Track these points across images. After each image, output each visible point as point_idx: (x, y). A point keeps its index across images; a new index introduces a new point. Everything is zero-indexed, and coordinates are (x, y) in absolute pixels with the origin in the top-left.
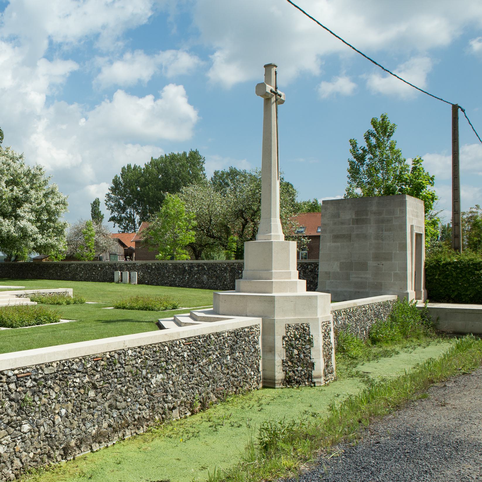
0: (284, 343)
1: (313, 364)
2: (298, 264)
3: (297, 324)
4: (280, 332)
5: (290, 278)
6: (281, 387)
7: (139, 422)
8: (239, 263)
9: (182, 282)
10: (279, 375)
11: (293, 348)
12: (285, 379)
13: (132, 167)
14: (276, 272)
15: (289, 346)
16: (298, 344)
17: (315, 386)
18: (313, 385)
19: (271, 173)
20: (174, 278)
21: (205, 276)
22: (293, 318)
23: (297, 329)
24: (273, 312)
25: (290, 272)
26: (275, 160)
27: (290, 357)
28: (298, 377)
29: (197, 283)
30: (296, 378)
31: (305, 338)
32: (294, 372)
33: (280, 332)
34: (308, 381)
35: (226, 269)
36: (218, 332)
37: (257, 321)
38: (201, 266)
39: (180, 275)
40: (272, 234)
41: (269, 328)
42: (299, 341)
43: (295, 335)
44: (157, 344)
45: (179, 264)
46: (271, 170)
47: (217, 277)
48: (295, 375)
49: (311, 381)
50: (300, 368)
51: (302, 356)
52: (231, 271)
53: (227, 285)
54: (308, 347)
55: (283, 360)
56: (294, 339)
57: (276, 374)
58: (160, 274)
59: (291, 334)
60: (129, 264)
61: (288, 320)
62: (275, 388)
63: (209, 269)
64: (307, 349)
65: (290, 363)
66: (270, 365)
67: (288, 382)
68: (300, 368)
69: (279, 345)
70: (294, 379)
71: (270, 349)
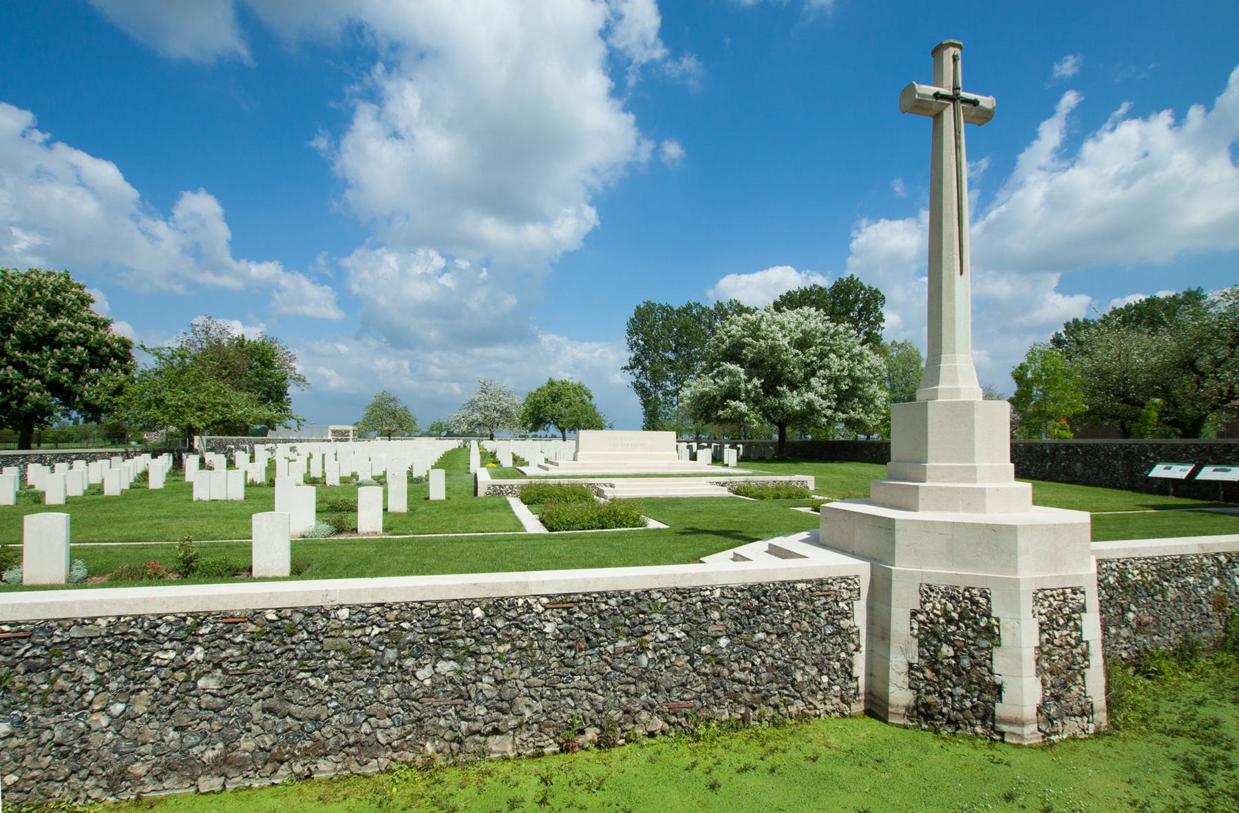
0: (916, 626)
1: (999, 689)
2: (1014, 448)
3: (955, 588)
4: (903, 601)
5: (974, 480)
6: (901, 722)
8: (1141, 445)
10: (900, 695)
11: (940, 640)
12: (916, 707)
14: (936, 467)
15: (929, 636)
16: (953, 633)
17: (1002, 741)
18: (997, 737)
19: (941, 262)
21: (1079, 465)
22: (943, 572)
23: (952, 598)
24: (891, 556)
25: (975, 467)
26: (951, 235)
28: (954, 709)
29: (1066, 474)
30: (945, 710)
31: (977, 623)
32: (941, 696)
33: (903, 601)
34: (983, 725)
35: (1116, 453)
36: (679, 586)
37: (861, 569)
38: (1073, 448)
40: (940, 387)
41: (881, 589)
42: (959, 628)
43: (946, 613)
44: (440, 601)
45: (1036, 444)
46: (941, 257)
47: (1099, 467)
48: (945, 704)
49: (993, 728)
50: (960, 691)
51: (966, 662)
52: (1125, 458)
53: (1117, 479)
54: (984, 644)
55: (911, 666)
56: (942, 620)
57: (891, 689)
59: (934, 607)
61: (929, 575)
62: (885, 721)
63: (1085, 453)
65: (929, 674)
66: (878, 669)
67: (922, 713)
68: (960, 691)
69: (901, 626)
70: (941, 713)
71: (880, 631)
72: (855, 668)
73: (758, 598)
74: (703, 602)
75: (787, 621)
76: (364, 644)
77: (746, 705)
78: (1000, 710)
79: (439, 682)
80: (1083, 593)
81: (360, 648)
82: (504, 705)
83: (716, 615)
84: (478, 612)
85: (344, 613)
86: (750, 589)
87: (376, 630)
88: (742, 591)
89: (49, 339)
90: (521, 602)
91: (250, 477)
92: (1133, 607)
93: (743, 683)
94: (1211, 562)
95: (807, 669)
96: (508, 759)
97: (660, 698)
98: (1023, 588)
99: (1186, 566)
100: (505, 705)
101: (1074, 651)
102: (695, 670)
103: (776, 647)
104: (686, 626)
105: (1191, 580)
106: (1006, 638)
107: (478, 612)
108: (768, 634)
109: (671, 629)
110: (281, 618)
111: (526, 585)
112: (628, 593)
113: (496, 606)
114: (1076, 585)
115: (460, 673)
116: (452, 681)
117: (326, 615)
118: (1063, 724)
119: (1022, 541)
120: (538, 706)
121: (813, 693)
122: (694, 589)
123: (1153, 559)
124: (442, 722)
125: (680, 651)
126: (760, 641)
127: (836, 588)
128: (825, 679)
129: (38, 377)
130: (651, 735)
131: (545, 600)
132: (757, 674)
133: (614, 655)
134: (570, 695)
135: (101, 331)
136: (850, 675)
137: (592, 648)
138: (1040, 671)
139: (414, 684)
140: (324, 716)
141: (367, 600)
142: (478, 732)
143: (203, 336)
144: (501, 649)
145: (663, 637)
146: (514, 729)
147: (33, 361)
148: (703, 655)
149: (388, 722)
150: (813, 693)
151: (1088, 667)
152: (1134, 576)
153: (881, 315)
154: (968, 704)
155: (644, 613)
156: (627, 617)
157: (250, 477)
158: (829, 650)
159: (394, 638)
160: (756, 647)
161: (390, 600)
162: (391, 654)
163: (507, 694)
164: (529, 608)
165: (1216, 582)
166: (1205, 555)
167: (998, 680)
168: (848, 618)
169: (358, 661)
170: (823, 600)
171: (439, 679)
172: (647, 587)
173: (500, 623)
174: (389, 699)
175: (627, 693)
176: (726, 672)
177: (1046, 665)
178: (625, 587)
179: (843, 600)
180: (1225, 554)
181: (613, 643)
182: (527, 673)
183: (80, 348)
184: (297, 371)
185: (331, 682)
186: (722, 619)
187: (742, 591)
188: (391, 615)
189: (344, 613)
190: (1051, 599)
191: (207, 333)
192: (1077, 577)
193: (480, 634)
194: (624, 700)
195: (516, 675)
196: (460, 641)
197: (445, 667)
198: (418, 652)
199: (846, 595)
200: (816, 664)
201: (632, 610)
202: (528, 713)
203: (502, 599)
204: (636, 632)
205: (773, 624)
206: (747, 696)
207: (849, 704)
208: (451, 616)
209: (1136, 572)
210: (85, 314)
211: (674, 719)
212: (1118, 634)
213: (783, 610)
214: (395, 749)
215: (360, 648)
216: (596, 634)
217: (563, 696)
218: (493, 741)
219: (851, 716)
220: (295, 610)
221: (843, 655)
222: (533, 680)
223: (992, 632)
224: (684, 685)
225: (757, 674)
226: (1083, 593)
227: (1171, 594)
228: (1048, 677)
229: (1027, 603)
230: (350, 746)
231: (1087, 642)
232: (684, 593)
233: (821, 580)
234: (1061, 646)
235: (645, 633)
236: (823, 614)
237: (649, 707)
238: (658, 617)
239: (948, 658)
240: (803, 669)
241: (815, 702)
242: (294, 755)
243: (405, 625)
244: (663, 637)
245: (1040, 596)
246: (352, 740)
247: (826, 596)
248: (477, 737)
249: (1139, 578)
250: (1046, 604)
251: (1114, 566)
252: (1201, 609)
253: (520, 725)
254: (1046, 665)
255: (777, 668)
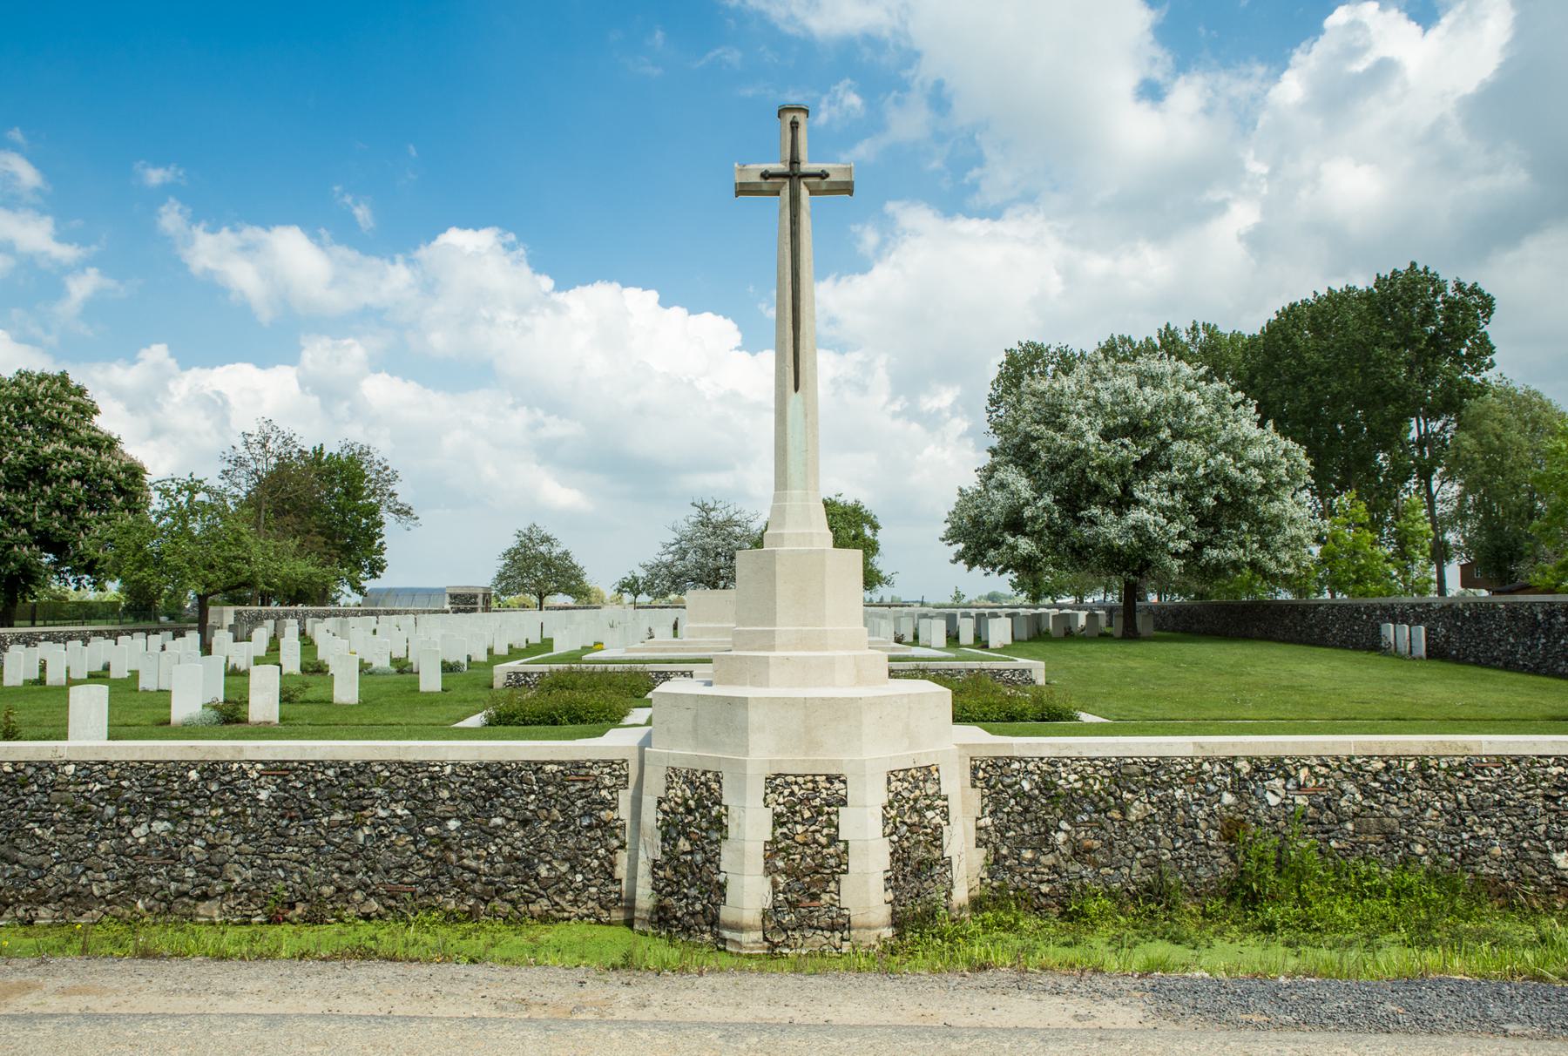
1: (722, 887)
7: (78, 899)
9: (1532, 658)
13: (1420, 268)
15: (670, 830)
20: (1513, 646)
27: (671, 857)
39: (1525, 635)
50: (693, 892)
54: (715, 836)
58: (1480, 631)
60: (1419, 605)
61: (674, 757)
64: (711, 843)
67: (662, 918)
72: (618, 869)
73: (496, 778)
74: (431, 778)
75: (532, 807)
76: (86, 799)
77: (475, 897)
78: (726, 914)
79: (153, 840)
80: (844, 782)
81: (82, 802)
82: (212, 868)
83: (445, 794)
84: (193, 775)
85: (71, 769)
86: (487, 767)
87: (98, 786)
88: (478, 769)
89: (38, 471)
90: (236, 766)
91: (231, 662)
92: (1064, 825)
93: (475, 871)
94: (1217, 769)
95: (555, 863)
96: (214, 924)
97: (376, 878)
98: (749, 771)
99: (1168, 772)
100: (215, 869)
101: (825, 851)
102: (418, 852)
103: (517, 835)
104: (410, 804)
105: (1179, 793)
106: (732, 832)
107: (193, 775)
108: (509, 820)
109: (393, 806)
110: (16, 771)
111: (241, 750)
112: (347, 763)
113: (211, 770)
114: (834, 772)
115: (173, 833)
116: (165, 842)
117: (54, 769)
118: (804, 937)
119: (754, 716)
120: (249, 874)
121: (562, 892)
122: (421, 763)
123: (1104, 760)
124: (153, 881)
125: (402, 830)
126: (496, 827)
127: (596, 773)
128: (579, 877)
129: (23, 526)
130: (367, 917)
131: (259, 766)
132: (492, 863)
133: (329, 827)
134: (281, 866)
135: (104, 458)
136: (611, 875)
137: (305, 819)
138: (770, 870)
139: (129, 841)
140: (46, 865)
141: (92, 758)
142: (186, 894)
143: (258, 450)
144: (214, 813)
145: (382, 813)
146: (222, 895)
147: (19, 504)
148: (429, 837)
149: (104, 876)
150: (562, 892)
151: (846, 872)
152: (1068, 780)
153: (1484, 339)
154: (698, 907)
155: (364, 786)
156: (344, 789)
157: (231, 662)
158: (585, 844)
159: (114, 794)
160: (492, 834)
161: (112, 758)
162: (110, 810)
163: (217, 858)
164: (244, 774)
165: (1228, 798)
166: (1206, 759)
167: (721, 878)
168: (612, 810)
169: (80, 814)
170: (579, 785)
171: (152, 838)
172: (368, 758)
173: (214, 787)
174: (107, 854)
175: (339, 869)
176: (453, 857)
177: (781, 864)
178: (344, 758)
179: (605, 787)
180: (1250, 760)
181: (329, 815)
182: (238, 840)
183: (75, 483)
184: (400, 499)
185: (56, 832)
186: (452, 799)
187: (478, 769)
188: (112, 774)
189: (71, 769)
190: (796, 788)
191: (264, 446)
192: (833, 762)
193: (195, 796)
194: (336, 876)
195: (227, 840)
196: (175, 803)
197: (158, 827)
198: (135, 810)
199: (607, 781)
200: (566, 860)
201: (350, 782)
202: (238, 880)
203: (217, 762)
204: (356, 805)
205: (515, 810)
206: (477, 887)
207: (608, 910)
208: (168, 778)
209: (1072, 777)
210: (84, 433)
211: (393, 903)
212: (1033, 862)
213: (528, 795)
214: (109, 903)
215: (82, 802)
216: (311, 805)
217: (274, 867)
218: (202, 908)
219: (609, 924)
220: (28, 764)
221: (602, 852)
222: (244, 846)
223: (721, 822)
224: (405, 867)
225: (492, 863)
226: (844, 782)
227: (1135, 813)
228: (782, 880)
229: (756, 789)
230: (68, 895)
231: (846, 842)
232: (409, 767)
233: (576, 762)
234: (805, 844)
235: (364, 808)
236: (579, 803)
237: (362, 886)
238: (379, 791)
239: (684, 853)
240: (549, 862)
241: (564, 904)
242: (17, 900)
243: (125, 783)
244: (382, 813)
245: (774, 783)
246: (69, 889)
247: (584, 781)
248: (186, 900)
249: (1078, 785)
250: (786, 792)
251: (1031, 767)
252: (1194, 836)
253: (228, 890)
254: (781, 864)
255: (517, 859)
